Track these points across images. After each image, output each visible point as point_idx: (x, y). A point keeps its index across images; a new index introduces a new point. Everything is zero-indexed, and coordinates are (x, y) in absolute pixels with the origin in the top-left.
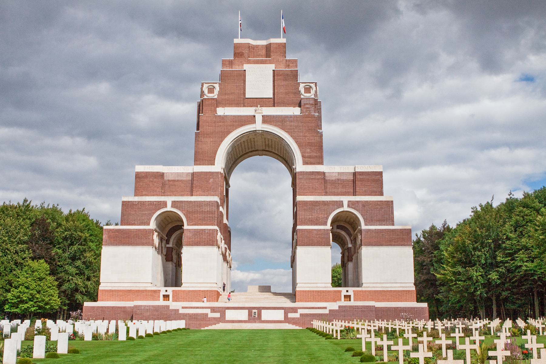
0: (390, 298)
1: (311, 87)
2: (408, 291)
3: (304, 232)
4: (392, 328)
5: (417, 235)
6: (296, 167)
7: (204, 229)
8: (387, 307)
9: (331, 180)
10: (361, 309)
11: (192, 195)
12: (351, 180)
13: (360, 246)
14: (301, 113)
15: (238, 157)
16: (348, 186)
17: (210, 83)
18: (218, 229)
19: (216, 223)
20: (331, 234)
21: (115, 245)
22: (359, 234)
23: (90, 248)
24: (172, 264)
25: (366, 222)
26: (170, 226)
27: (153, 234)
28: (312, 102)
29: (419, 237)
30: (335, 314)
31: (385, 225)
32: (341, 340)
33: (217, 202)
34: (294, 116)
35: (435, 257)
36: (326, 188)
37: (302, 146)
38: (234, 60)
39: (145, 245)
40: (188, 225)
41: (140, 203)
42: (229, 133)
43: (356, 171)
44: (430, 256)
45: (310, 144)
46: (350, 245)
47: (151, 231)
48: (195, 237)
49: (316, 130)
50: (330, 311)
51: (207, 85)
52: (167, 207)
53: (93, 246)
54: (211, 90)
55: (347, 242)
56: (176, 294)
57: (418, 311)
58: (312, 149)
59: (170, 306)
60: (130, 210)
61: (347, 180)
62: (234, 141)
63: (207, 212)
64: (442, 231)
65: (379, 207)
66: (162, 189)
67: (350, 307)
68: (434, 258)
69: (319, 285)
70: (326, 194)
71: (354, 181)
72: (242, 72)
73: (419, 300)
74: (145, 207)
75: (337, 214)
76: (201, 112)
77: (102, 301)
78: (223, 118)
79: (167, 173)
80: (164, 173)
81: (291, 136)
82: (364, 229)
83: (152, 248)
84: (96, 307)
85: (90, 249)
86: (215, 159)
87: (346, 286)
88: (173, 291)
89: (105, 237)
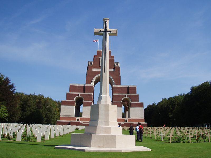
11: (85, 92)
88: (80, 118)
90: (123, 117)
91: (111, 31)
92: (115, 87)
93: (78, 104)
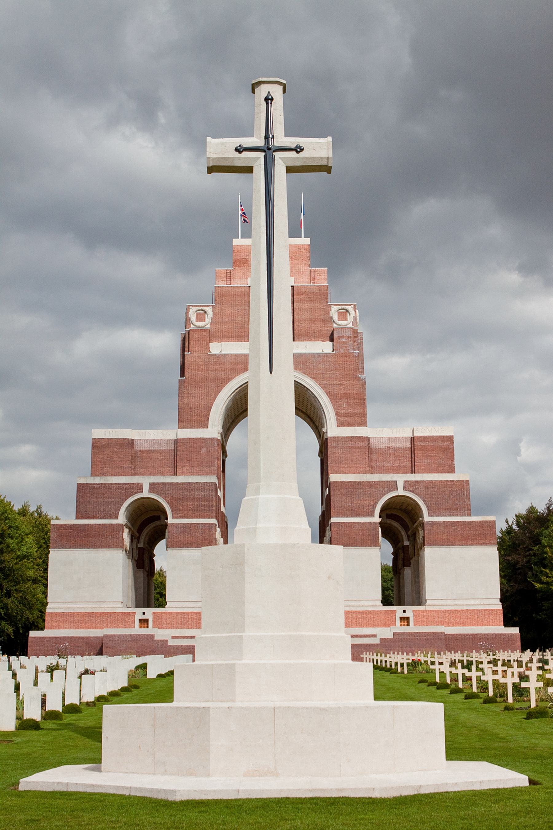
0: (466, 620)
1: (347, 311)
2: (492, 610)
3: (342, 526)
4: (467, 660)
5: (507, 522)
6: (327, 429)
7: (198, 524)
8: (461, 634)
9: (379, 448)
10: (425, 636)
11: (175, 474)
12: (407, 449)
13: (421, 546)
14: (333, 351)
15: (240, 412)
16: (403, 457)
17: (198, 306)
18: (217, 523)
19: (214, 515)
20: (380, 529)
21: (68, 548)
22: (420, 529)
23: (8, 547)
24: (144, 573)
25: (430, 512)
26: (144, 518)
27: (123, 532)
28: (350, 333)
29: (510, 524)
30: (389, 645)
31: (457, 515)
32: (408, 674)
33: (215, 484)
34: (324, 355)
35: (535, 555)
36: (370, 460)
37: (336, 399)
38: (233, 270)
39: (111, 548)
40: (173, 518)
41: (103, 486)
42: (228, 380)
43: (415, 435)
44: (528, 553)
45: (347, 396)
46: (406, 543)
47: (120, 527)
48: (184, 534)
49: (356, 376)
50: (381, 640)
51: (195, 309)
52: (142, 492)
53: (12, 544)
54: (201, 316)
55: (402, 538)
56: (158, 618)
57: (505, 640)
58: (350, 403)
59: (155, 636)
60: (90, 497)
61: (401, 448)
62: (235, 392)
63: (202, 498)
64: (545, 515)
65: (449, 489)
66: (132, 464)
67: (410, 634)
68: (533, 557)
69: (363, 603)
70: (372, 470)
71: (412, 450)
72: (246, 289)
73: (507, 623)
74: (111, 492)
75: (388, 499)
76: (186, 349)
77: (51, 628)
78: (220, 357)
79: (138, 440)
80: (133, 440)
81: (320, 385)
82: (428, 522)
83: (121, 551)
84: (47, 637)
85: (9, 550)
86: (208, 419)
87: (400, 604)
89: (52, 535)
90: (386, 601)
91: (298, 149)
92: (337, 439)
93: (138, 539)
